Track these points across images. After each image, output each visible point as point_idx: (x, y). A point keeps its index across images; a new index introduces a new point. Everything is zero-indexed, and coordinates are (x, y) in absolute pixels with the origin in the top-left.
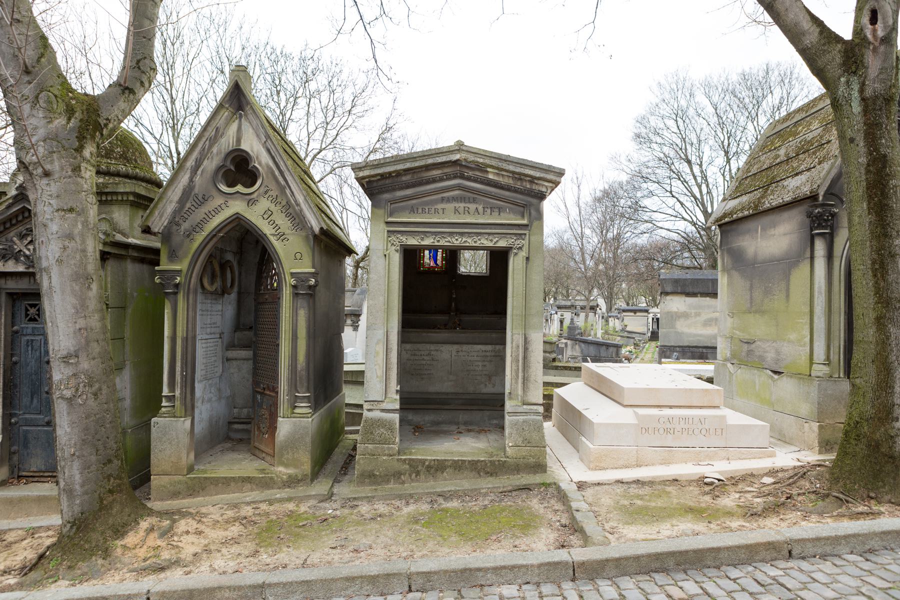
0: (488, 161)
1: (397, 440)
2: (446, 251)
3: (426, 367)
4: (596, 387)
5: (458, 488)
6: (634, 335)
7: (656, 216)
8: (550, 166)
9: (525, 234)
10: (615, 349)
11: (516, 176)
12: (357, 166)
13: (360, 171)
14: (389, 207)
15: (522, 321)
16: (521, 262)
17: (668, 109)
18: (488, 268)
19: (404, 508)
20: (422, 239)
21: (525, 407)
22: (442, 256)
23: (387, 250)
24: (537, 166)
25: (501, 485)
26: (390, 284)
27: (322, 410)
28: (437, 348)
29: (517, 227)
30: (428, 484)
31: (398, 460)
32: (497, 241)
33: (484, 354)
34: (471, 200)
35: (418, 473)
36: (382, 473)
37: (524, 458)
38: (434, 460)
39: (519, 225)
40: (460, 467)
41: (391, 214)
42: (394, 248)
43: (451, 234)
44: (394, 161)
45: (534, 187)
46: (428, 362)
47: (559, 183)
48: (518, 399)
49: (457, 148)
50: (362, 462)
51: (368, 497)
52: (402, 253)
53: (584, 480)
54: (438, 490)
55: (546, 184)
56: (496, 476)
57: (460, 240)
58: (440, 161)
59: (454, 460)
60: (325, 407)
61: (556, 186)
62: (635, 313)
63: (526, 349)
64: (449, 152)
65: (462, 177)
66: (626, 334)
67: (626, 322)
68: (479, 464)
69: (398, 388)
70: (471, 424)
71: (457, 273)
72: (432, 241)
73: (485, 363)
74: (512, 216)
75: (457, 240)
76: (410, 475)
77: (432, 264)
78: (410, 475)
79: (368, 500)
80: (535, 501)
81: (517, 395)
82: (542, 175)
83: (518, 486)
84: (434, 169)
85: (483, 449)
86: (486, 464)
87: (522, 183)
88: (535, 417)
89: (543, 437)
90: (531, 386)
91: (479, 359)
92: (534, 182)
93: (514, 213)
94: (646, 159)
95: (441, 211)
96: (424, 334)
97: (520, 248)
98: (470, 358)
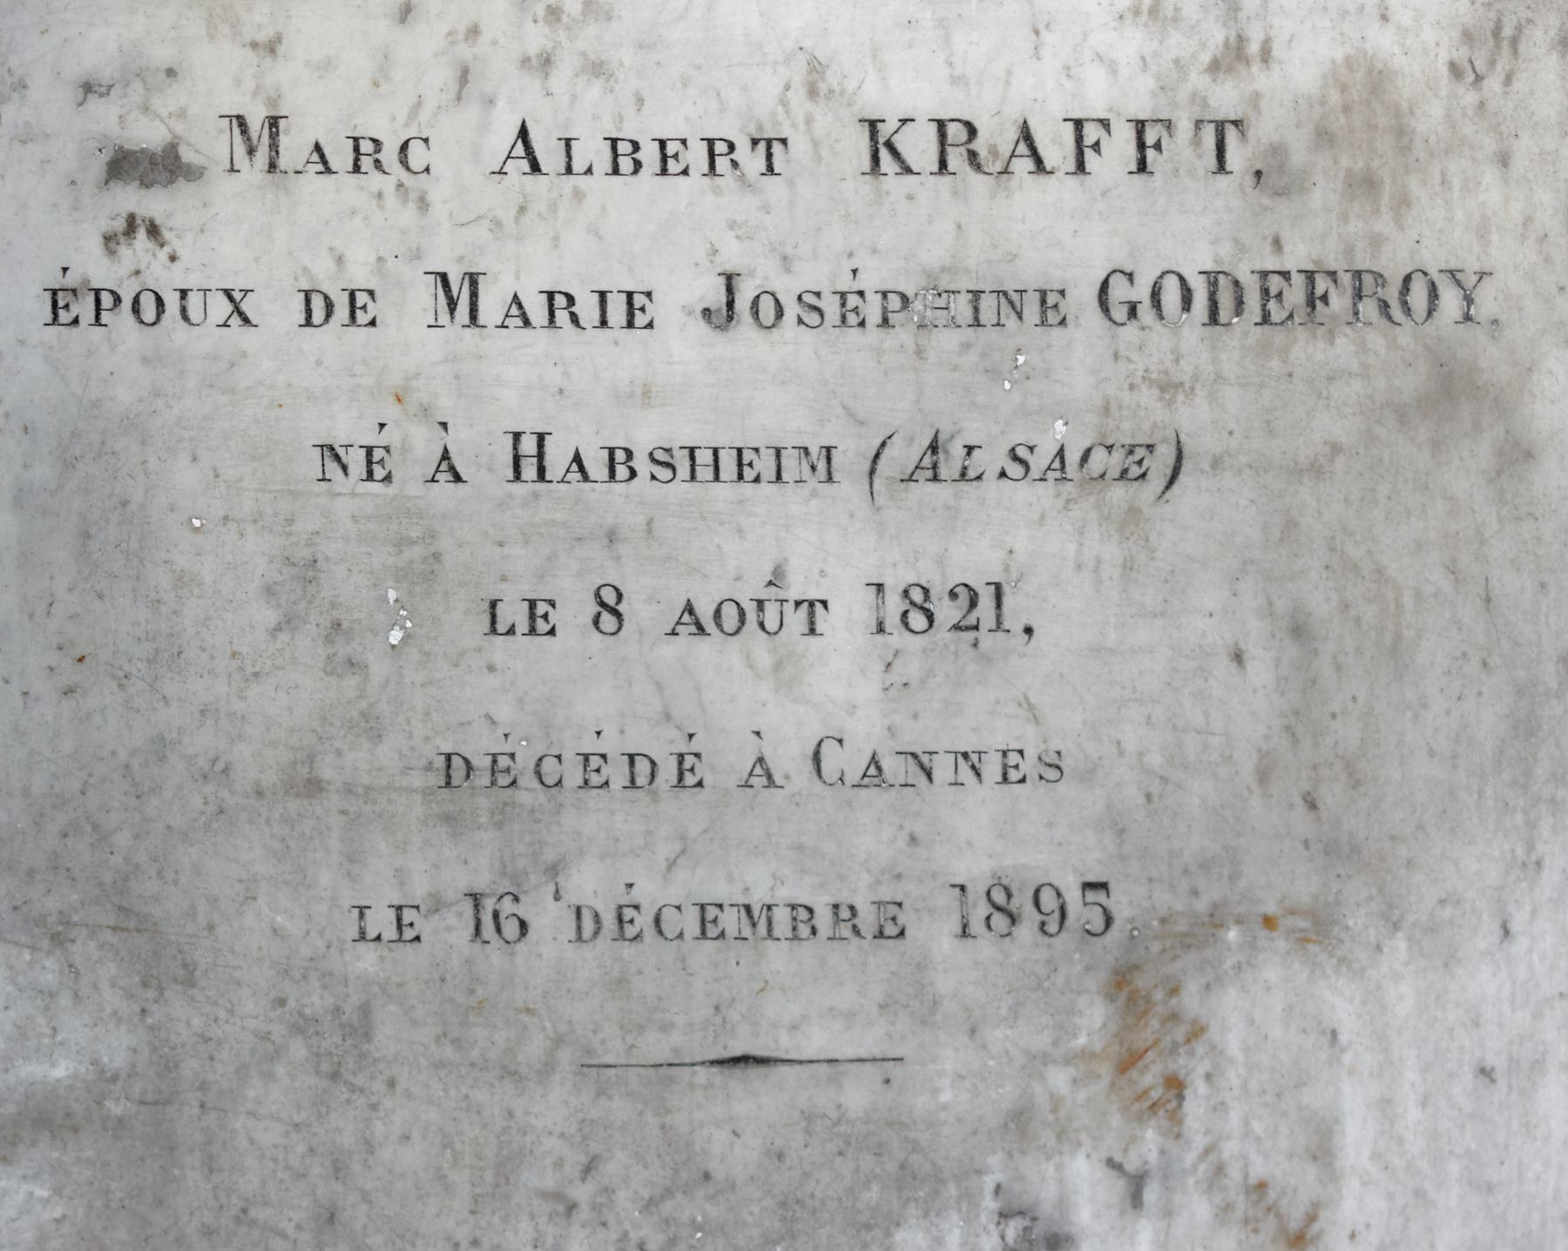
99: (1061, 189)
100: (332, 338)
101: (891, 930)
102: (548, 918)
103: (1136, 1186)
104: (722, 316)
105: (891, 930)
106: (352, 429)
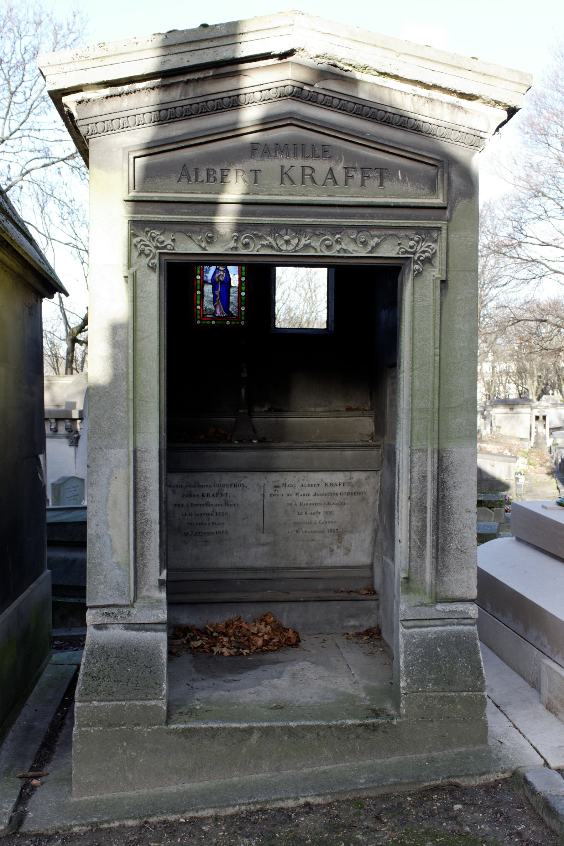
3: (212, 519)
9: (439, 229)
21: (440, 607)
26: (139, 345)
28: (235, 481)
32: (378, 245)
33: (329, 490)
34: (319, 152)
42: (145, 261)
43: (275, 229)
46: (218, 509)
57: (296, 241)
73: (332, 508)
74: (409, 187)
91: (318, 499)
97: (428, 261)
98: (301, 499)
99: (338, 487)
100: (289, 497)
101: (323, 532)
102: (301, 531)
104: (315, 495)
105: (323, 532)
106: (289, 502)
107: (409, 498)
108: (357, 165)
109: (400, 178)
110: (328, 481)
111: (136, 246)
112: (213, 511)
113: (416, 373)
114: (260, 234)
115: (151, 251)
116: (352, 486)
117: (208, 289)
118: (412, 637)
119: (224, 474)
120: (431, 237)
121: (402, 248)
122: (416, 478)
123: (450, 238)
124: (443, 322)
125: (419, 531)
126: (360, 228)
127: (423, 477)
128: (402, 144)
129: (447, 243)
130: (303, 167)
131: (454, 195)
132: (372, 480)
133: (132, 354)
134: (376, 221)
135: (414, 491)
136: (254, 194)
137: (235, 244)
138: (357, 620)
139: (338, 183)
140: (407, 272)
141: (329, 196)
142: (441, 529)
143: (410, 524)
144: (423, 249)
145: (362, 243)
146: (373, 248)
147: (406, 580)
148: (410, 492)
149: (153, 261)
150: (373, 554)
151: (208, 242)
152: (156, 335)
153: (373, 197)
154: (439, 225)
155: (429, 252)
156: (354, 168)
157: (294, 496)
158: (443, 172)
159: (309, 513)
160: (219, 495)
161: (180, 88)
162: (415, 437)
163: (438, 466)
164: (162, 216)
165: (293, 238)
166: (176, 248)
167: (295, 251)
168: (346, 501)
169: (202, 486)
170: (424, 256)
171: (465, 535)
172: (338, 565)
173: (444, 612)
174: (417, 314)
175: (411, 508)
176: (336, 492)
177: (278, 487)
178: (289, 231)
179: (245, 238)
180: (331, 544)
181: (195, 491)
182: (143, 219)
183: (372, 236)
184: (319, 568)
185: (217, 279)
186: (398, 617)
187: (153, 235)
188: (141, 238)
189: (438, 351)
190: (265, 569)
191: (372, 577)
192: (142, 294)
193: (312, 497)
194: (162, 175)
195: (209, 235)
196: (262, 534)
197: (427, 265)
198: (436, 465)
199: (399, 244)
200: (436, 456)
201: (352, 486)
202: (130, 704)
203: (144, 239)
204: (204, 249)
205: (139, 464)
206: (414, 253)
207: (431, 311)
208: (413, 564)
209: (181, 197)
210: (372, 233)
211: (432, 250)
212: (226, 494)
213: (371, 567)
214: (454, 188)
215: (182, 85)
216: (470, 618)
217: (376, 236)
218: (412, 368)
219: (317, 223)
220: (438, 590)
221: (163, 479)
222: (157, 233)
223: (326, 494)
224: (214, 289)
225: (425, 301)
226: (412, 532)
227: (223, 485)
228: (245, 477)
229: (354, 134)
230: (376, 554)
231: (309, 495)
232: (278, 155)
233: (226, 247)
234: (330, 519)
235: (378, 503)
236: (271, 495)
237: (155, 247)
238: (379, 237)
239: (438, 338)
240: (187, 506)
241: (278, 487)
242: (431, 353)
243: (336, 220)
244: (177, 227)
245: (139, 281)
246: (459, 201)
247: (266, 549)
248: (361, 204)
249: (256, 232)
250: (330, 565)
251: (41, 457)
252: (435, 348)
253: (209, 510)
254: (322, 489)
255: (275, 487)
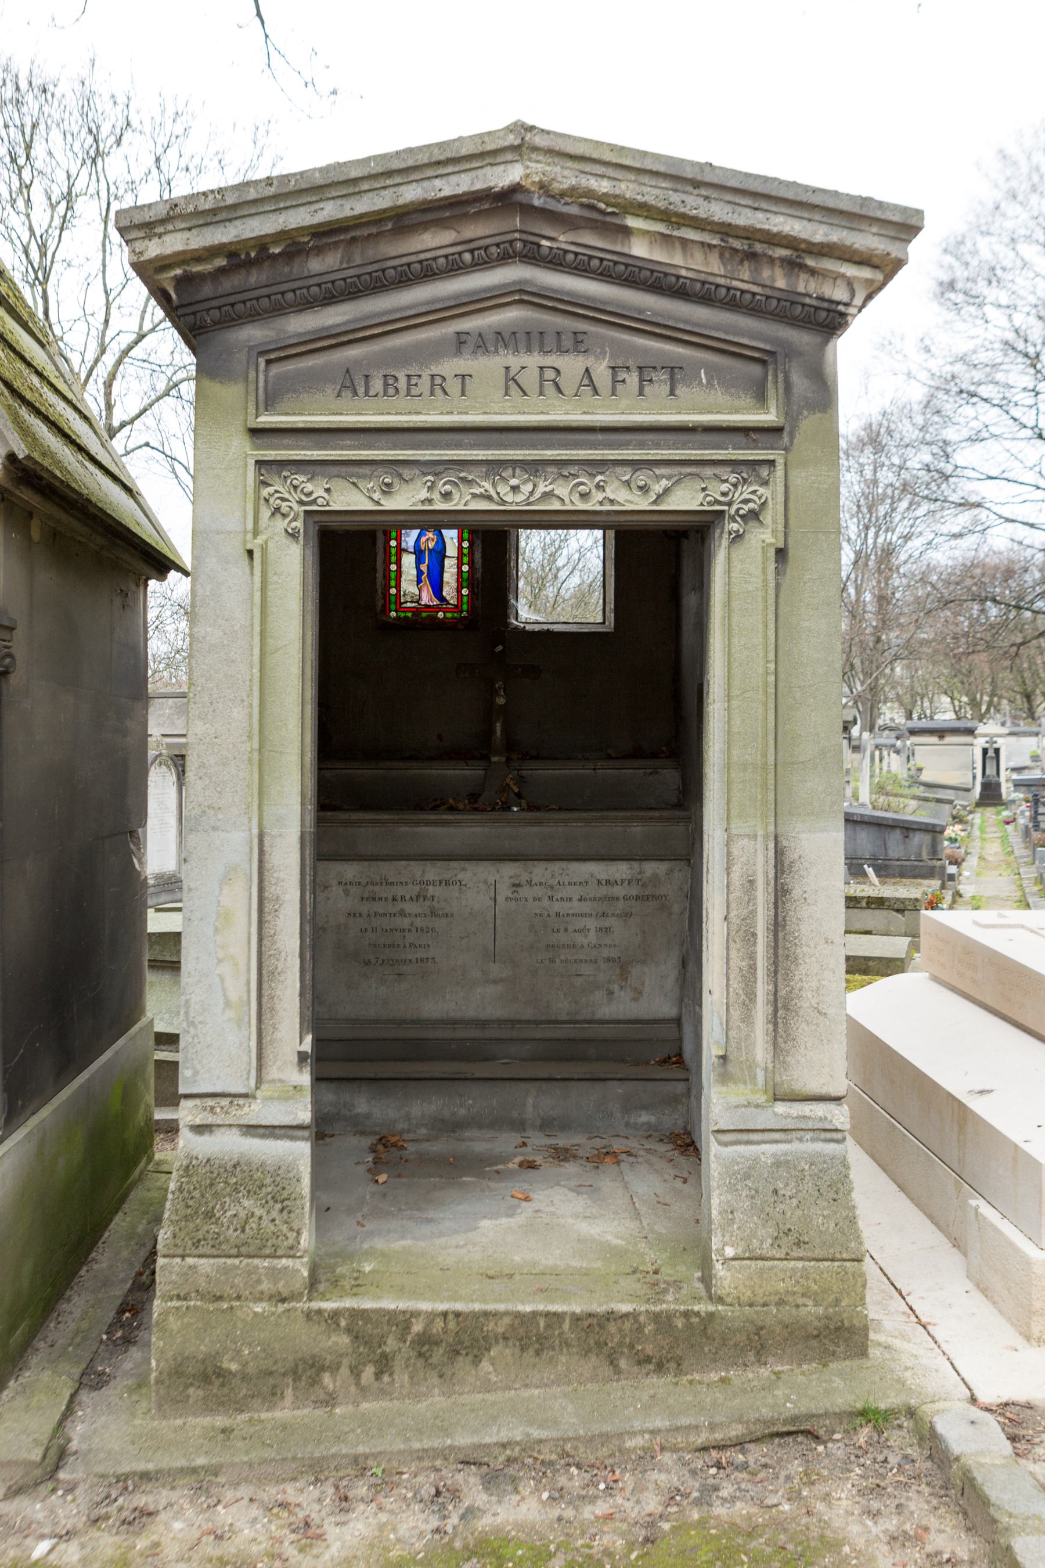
0: (628, 189)
1: (306, 1240)
2: (471, 532)
3: (410, 938)
4: (989, 1001)
5: (536, 1433)
6: (948, 795)
7: (987, 491)
8: (866, 201)
9: (771, 463)
10: (926, 839)
11: (736, 244)
12: (138, 219)
13: (149, 237)
14: (262, 374)
15: (765, 786)
16: (756, 570)
17: (1025, 216)
18: (611, 605)
19: (332, 1531)
20: (387, 490)
21: (781, 1108)
22: (460, 572)
23: (256, 533)
24: (816, 200)
25: (703, 1420)
27: (45, 1112)
28: (447, 876)
29: (740, 438)
30: (422, 1406)
31: (309, 1315)
32: (667, 491)
33: (604, 891)
34: (567, 342)
35: (384, 1365)
36: (251, 1369)
37: (781, 1303)
38: (445, 1314)
39: (745, 431)
40: (541, 1339)
41: (270, 402)
42: (281, 524)
43: (494, 468)
44: (276, 197)
45: (804, 284)
46: (419, 922)
47: (899, 264)
48: (753, 1079)
49: (512, 139)
50: (174, 1324)
51: (194, 1470)
52: (314, 542)
53: (1021, 1397)
54: (463, 1440)
55: (850, 270)
56: (679, 1372)
57: (529, 487)
58: (447, 192)
59: (517, 1315)
60: (65, 1094)
61: (889, 277)
62: (941, 737)
63: (781, 894)
64: (482, 155)
65: (533, 256)
66: (920, 791)
67: (919, 760)
68: (612, 1328)
69: (307, 1045)
70: (564, 1125)
71: (507, 624)
72: (424, 494)
74: (718, 396)
75: (515, 489)
76: (356, 1372)
77: (427, 597)
78: (356, 1372)
79: (191, 1480)
80: (844, 1496)
81: (751, 1066)
82: (836, 236)
83: (766, 1423)
84: (424, 226)
85: (619, 1254)
86: (640, 1329)
87: (757, 271)
88: (819, 1147)
89: (853, 1221)
90: (802, 1030)
91: (586, 907)
92: (802, 267)
93: (728, 383)
94: (969, 346)
95: (453, 386)
96: (404, 829)
97: (754, 516)
98: (557, 907)
99: (620, 887)
100: (537, 903)
101: (596, 962)
102: (558, 961)
103: (622, 988)
104: (580, 900)
105: (596, 962)
106: (538, 912)
107: (726, 918)
108: (630, 363)
109: (704, 381)
110: (603, 876)
111: (267, 500)
112: (412, 925)
113: (735, 703)
114: (470, 477)
115: (290, 507)
116: (644, 885)
117: (409, 561)
118: (735, 1162)
119: (428, 863)
120: (758, 476)
121: (708, 495)
122: (737, 883)
123: (790, 478)
124: (781, 619)
125: (743, 976)
126: (636, 465)
127: (750, 881)
128: (706, 327)
129: (786, 486)
130: (541, 368)
131: (795, 407)
132: (677, 875)
133: (258, 675)
134: (664, 452)
135: (733, 906)
136: (459, 413)
137: (428, 495)
138: (653, 1114)
139: (599, 393)
140: (717, 535)
141: (584, 413)
142: (781, 972)
143: (727, 963)
144: (745, 496)
145: (640, 488)
146: (659, 496)
147: (721, 1061)
148: (728, 907)
149: (294, 524)
150: (681, 1001)
151: (384, 492)
152: (297, 645)
153: (658, 414)
154: (771, 458)
155: (755, 502)
156: (627, 368)
157: (546, 902)
158: (776, 370)
159: (570, 928)
160: (422, 899)
161: (340, 250)
162: (734, 812)
163: (776, 862)
164: (309, 453)
165: (525, 482)
166: (331, 503)
167: (528, 504)
168: (633, 910)
169: (392, 884)
170: (746, 508)
171: (824, 983)
172: (621, 1017)
173: (787, 1116)
174: (735, 604)
175: (728, 935)
176: (616, 895)
177: (519, 885)
178: (518, 471)
179: (445, 484)
180: (609, 982)
181: (381, 891)
182: (279, 458)
183: (657, 476)
184: (589, 1022)
185: (423, 547)
186: (708, 1125)
187: (295, 482)
188: (276, 488)
189: (772, 666)
190: (500, 1022)
191: (680, 1040)
192: (275, 578)
193: (575, 903)
194: (311, 388)
195: (386, 480)
196: (492, 964)
197: (752, 524)
198: (772, 862)
199: (704, 489)
200: (772, 845)
201: (644, 885)
202: (248, 1265)
203: (281, 489)
204: (378, 503)
205: (267, 856)
206: (729, 504)
207: (760, 600)
208: (733, 1033)
209: (340, 422)
210: (658, 471)
211: (760, 498)
212: (433, 897)
213: (678, 1021)
214: (796, 395)
215: (342, 246)
216: (836, 1130)
217: (663, 477)
218: (728, 696)
219: (564, 458)
220: (778, 1079)
221: (307, 882)
222: (301, 480)
223: (600, 899)
224: (419, 562)
225: (749, 582)
226: (732, 977)
227: (428, 883)
228: (464, 869)
229: (625, 313)
230: (686, 1000)
231: (570, 899)
232: (501, 350)
233: (414, 500)
234: (608, 941)
235: (687, 914)
236: (506, 899)
237: (297, 502)
238: (669, 478)
239: (773, 646)
240: (369, 915)
241: (519, 885)
242: (761, 671)
243: (597, 452)
244: (334, 470)
245: (271, 557)
246: (806, 417)
247: (499, 988)
248: (631, 425)
249: (462, 475)
250: (607, 1018)
251: (140, 830)
252: (768, 662)
253: (406, 922)
254: (592, 891)
255: (514, 885)
